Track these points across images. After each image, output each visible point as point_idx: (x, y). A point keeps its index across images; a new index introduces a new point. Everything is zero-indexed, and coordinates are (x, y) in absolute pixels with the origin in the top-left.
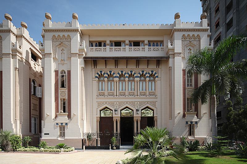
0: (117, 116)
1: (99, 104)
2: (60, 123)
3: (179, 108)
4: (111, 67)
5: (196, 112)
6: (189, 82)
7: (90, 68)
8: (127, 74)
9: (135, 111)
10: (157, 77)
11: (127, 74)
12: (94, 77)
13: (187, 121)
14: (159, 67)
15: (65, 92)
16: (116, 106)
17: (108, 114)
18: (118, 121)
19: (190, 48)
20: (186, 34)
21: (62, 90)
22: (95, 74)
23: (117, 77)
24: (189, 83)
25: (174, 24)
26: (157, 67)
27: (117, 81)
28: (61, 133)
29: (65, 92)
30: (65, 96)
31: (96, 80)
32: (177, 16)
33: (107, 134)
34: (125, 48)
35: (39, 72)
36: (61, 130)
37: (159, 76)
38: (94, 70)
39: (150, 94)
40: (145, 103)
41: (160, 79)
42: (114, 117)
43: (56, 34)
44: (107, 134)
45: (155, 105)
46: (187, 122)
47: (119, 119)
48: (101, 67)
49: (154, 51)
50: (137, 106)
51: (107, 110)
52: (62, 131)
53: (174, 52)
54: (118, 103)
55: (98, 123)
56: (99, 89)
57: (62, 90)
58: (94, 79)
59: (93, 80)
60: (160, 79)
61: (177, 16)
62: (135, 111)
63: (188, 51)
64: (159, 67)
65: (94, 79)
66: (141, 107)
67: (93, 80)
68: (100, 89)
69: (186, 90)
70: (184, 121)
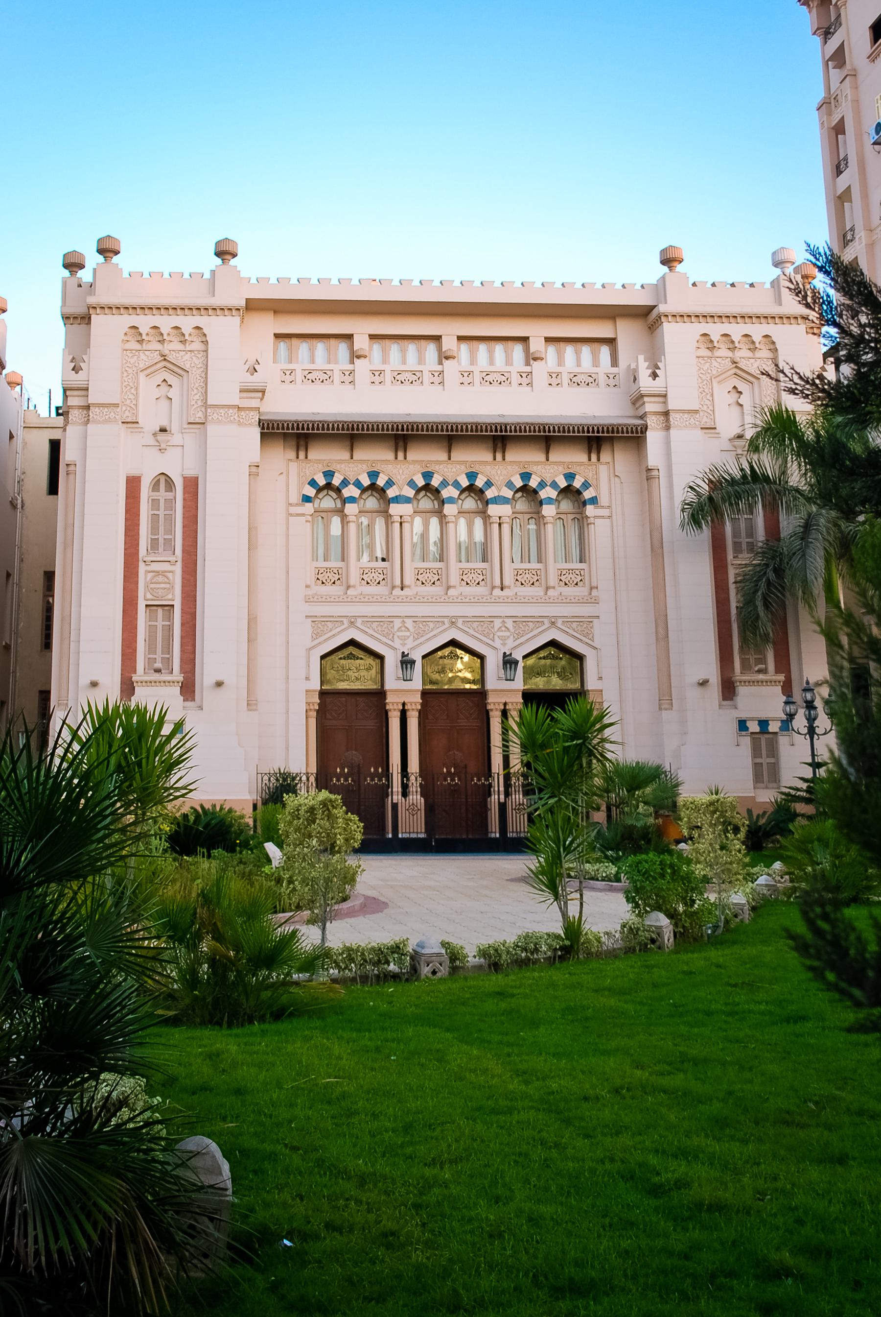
0: (404, 691)
1: (319, 623)
2: (752, 719)
3: (698, 655)
5: (781, 677)
6: (161, 529)
7: (281, 456)
9: (493, 663)
10: (594, 501)
11: (450, 487)
12: (295, 498)
13: (743, 715)
14: (599, 460)
16: (405, 638)
17: (357, 677)
18: (408, 714)
19: (735, 387)
20: (716, 330)
22: (301, 487)
23: (408, 500)
25: (660, 288)
26: (590, 460)
27: (505, 519)
28: (757, 767)
31: (303, 515)
32: (225, 252)
36: (756, 751)
37: (604, 500)
38: (294, 466)
40: (443, 623)
41: (606, 512)
42: (391, 691)
44: (338, 780)
45: (587, 634)
46: (742, 725)
47: (415, 701)
48: (326, 457)
50: (504, 639)
51: (351, 656)
52: (765, 760)
53: (665, 403)
54: (509, 623)
55: (313, 722)
56: (460, 557)
58: (293, 510)
59: (291, 515)
60: (606, 512)
61: (225, 252)
62: (493, 663)
63: (158, 393)
64: (599, 460)
65: (293, 510)
66: (581, 640)
67: (291, 515)
69: (142, 568)
70: (729, 717)
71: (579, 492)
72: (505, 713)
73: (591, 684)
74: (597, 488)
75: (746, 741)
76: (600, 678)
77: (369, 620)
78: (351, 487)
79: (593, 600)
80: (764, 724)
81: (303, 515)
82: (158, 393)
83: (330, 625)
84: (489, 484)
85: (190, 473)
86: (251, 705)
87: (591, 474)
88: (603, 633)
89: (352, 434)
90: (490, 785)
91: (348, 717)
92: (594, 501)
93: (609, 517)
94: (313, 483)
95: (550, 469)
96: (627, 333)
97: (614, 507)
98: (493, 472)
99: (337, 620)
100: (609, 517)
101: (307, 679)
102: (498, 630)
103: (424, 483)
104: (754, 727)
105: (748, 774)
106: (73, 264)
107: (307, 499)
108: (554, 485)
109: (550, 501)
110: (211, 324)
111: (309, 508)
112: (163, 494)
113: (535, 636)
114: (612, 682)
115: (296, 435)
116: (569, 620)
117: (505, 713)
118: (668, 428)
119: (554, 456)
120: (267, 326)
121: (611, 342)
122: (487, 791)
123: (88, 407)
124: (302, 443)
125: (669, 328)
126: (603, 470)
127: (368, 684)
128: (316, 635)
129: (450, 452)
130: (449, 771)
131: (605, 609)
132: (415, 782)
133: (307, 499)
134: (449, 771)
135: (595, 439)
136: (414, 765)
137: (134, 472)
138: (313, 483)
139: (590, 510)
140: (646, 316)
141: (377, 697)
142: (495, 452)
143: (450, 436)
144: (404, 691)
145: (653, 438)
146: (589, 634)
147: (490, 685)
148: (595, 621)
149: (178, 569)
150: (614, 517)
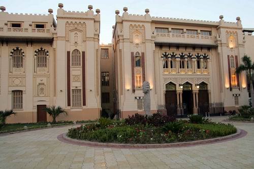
1: (165, 79)
4: (190, 50)
12: (160, 57)
36: (138, 103)
46: (136, 98)
48: (165, 50)
61: (147, 11)
63: (74, 35)
71: (191, 56)
72: (196, 94)
73: (209, 89)
75: (136, 100)
80: (140, 97)
82: (74, 35)
85: (143, 52)
86: (156, 93)
89: (170, 45)
91: (170, 94)
92: (209, 58)
94: (163, 54)
95: (202, 53)
96: (214, 31)
99: (201, 78)
104: (235, 95)
105: (234, 103)
106: (117, 13)
107: (162, 57)
109: (169, 57)
110: (145, 24)
111: (163, 59)
112: (232, 58)
114: (212, 88)
115: (160, 45)
117: (196, 94)
118: (221, 46)
119: (187, 50)
120: (155, 26)
121: (210, 32)
123: (221, 44)
125: (222, 29)
126: (210, 54)
127: (174, 89)
128: (164, 81)
133: (162, 57)
135: (209, 48)
136: (181, 102)
137: (68, 50)
138: (163, 54)
140: (217, 27)
141: (175, 91)
143: (186, 46)
144: (180, 89)
145: (219, 48)
149: (81, 69)
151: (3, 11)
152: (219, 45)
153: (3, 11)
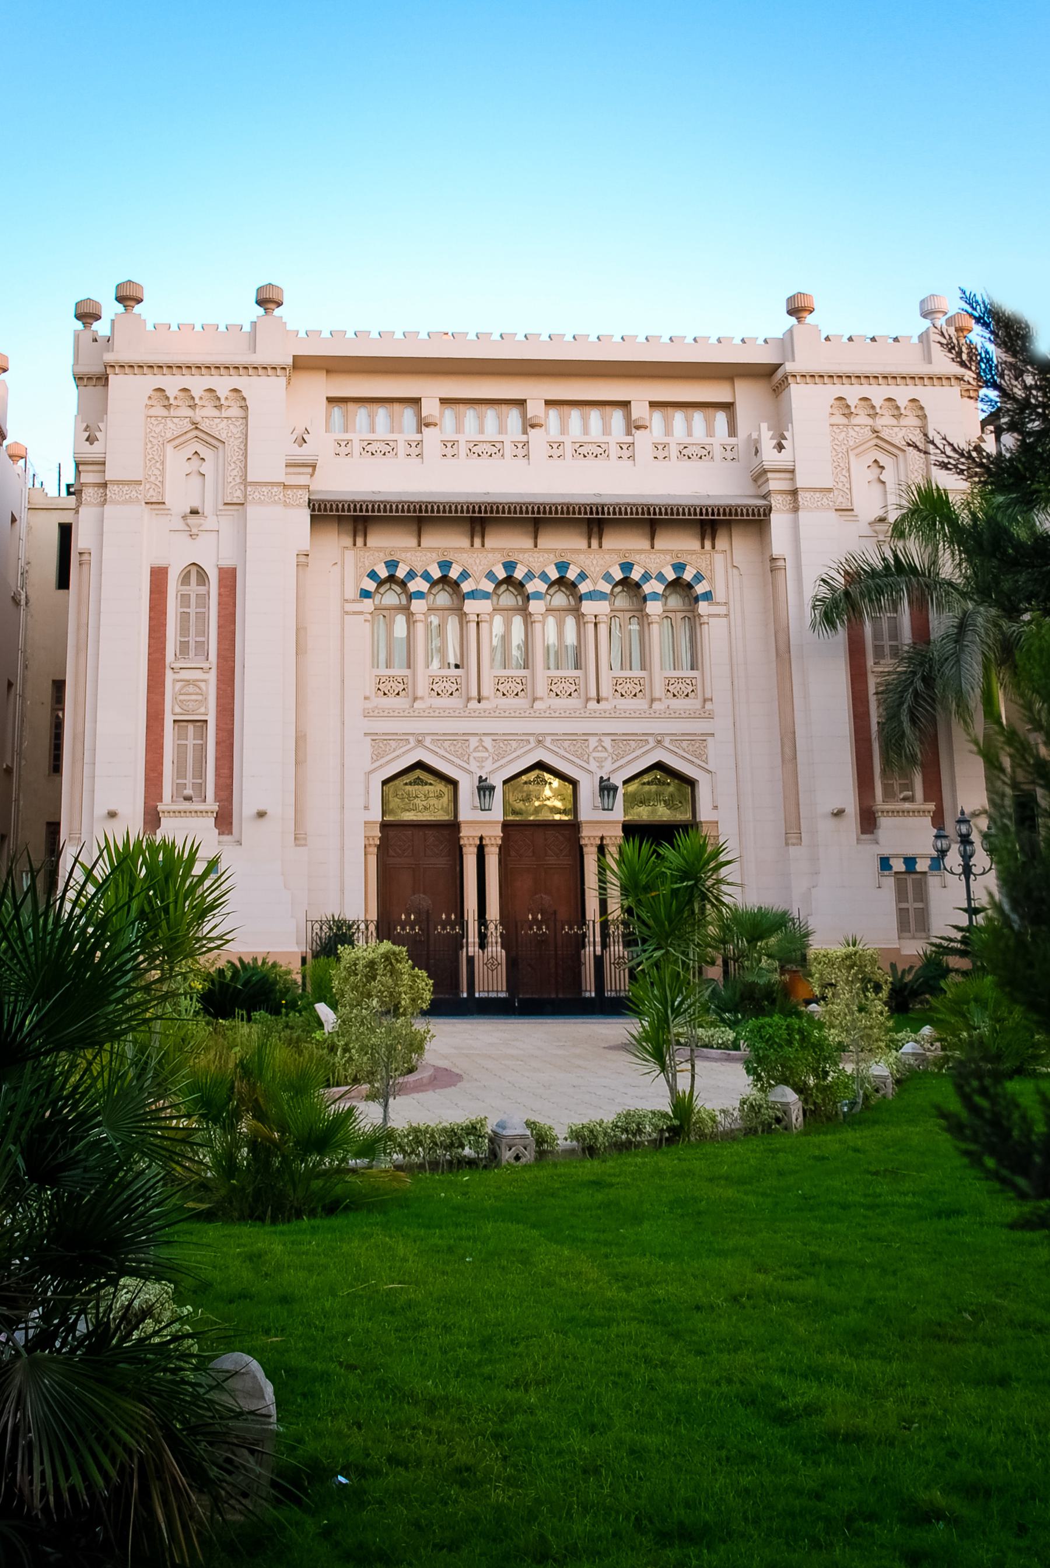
0: (481, 822)
1: (380, 742)
2: (897, 856)
3: (832, 780)
4: (565, 545)
5: (931, 806)
6: (192, 630)
8: (536, 580)
9: (588, 790)
10: (708, 596)
12: (352, 592)
13: (886, 852)
14: (713, 548)
15: (202, 685)
16: (483, 760)
17: (425, 806)
21: (185, 675)
22: (358, 580)
23: (486, 596)
24: (192, 640)
26: (703, 547)
27: (602, 618)
28: (902, 913)
29: (202, 685)
30: (202, 710)
31: (361, 613)
32: (268, 300)
33: (444, 928)
34: (526, 444)
35: (879, 565)
36: (901, 895)
37: (719, 595)
38: (350, 555)
39: (500, 687)
40: (528, 741)
41: (722, 610)
43: (172, 384)
45: (700, 755)
46: (885, 863)
47: (494, 835)
49: (476, 461)
50: (600, 761)
51: (419, 782)
52: (911, 905)
54: (607, 742)
55: (373, 860)
56: (548, 664)
57: (185, 675)
58: (349, 607)
59: (347, 613)
60: (722, 610)
61: (268, 300)
62: (588, 790)
63: (188, 467)
64: (713, 548)
65: (349, 607)
66: (621, 767)
67: (347, 613)
68: (382, 657)
69: (169, 676)
71: (690, 586)
72: (601, 849)
73: (705, 814)
74: (711, 581)
75: (890, 882)
76: (716, 808)
77: (440, 738)
78: (418, 579)
79: (706, 715)
80: (910, 862)
81: (361, 613)
82: (188, 467)
83: (393, 744)
84: (583, 576)
85: (227, 563)
86: (299, 839)
87: (704, 565)
88: (718, 753)
89: (420, 517)
90: (584, 935)
91: (415, 854)
92: (708, 596)
93: (726, 616)
94: (373, 575)
95: (655, 558)
96: (747, 397)
97: (731, 603)
98: (588, 562)
99: (402, 738)
100: (726, 616)
101: (366, 808)
102: (594, 750)
103: (505, 576)
104: (898, 866)
105: (892, 921)
106: (87, 315)
107: (366, 594)
108: (660, 577)
109: (655, 596)
110: (251, 386)
111: (368, 604)
112: (194, 589)
113: (637, 758)
114: (730, 812)
115: (353, 518)
116: (678, 739)
117: (601, 849)
118: (796, 509)
120: (318, 388)
121: (728, 407)
122: (581, 942)
123: (104, 485)
124: (360, 527)
125: (797, 391)
126: (719, 559)
127: (439, 814)
128: (376, 756)
129: (536, 538)
130: (535, 918)
131: (721, 726)
132: (494, 932)
133: (366, 594)
134: (535, 918)
135: (709, 523)
136: (493, 911)
137: (160, 563)
138: (373, 575)
139: (703, 607)
140: (770, 377)
141: (449, 830)
142: (355, 536)
143: (537, 519)
144: (481, 822)
145: (779, 521)
146: (702, 755)
147: (584, 815)
148: (709, 739)
150: (732, 616)
151: (87, 325)
152: (777, 502)
153: (87, 325)
